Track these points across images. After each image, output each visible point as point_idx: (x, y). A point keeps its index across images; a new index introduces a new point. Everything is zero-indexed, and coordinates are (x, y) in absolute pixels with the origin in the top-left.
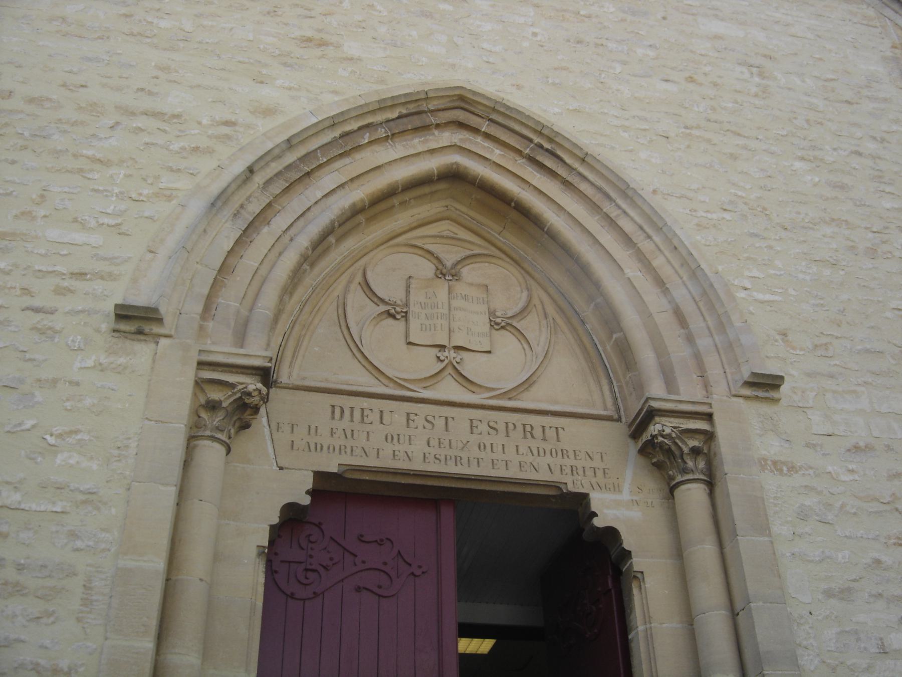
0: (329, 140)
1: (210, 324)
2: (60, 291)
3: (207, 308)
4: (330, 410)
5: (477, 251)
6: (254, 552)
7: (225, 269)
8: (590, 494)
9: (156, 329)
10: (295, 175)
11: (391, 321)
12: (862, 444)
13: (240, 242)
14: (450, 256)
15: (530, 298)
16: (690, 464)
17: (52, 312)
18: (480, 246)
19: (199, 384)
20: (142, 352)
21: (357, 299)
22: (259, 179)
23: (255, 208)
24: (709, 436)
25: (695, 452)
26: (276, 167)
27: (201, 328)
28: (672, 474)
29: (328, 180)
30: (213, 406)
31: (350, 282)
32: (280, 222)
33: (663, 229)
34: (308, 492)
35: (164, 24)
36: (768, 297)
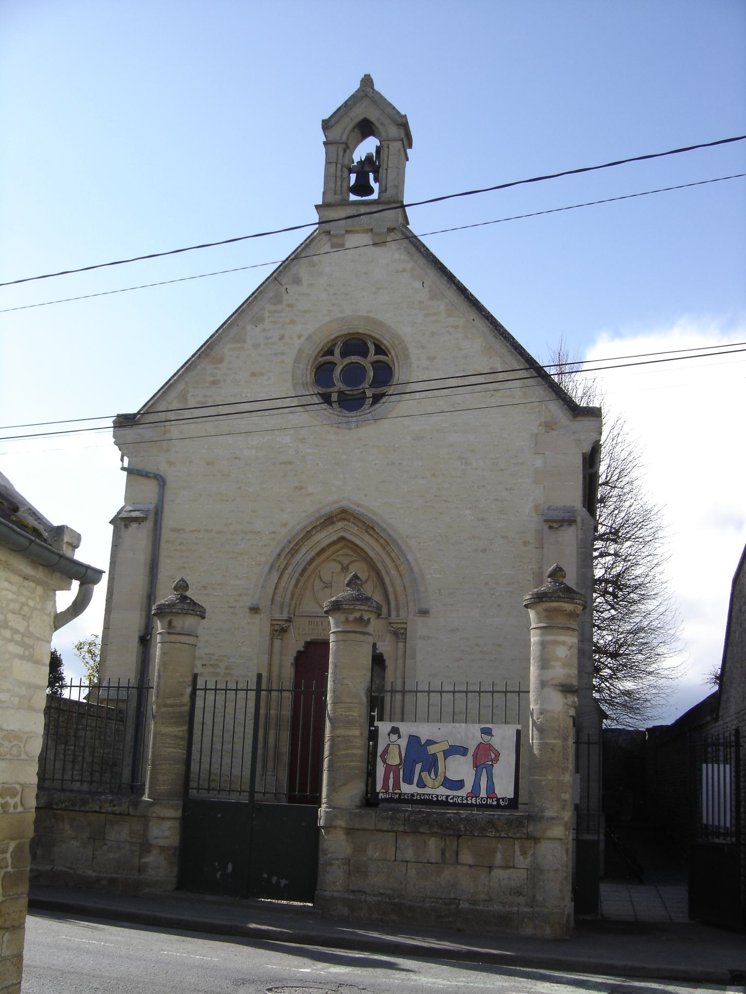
0: (302, 536)
1: (273, 606)
2: (236, 601)
3: (272, 602)
4: (308, 623)
5: (356, 559)
6: (290, 664)
7: (276, 588)
8: (377, 644)
9: (260, 612)
10: (293, 552)
11: (327, 589)
12: (454, 628)
13: (280, 578)
14: (346, 561)
15: (369, 575)
16: (401, 637)
17: (235, 607)
18: (355, 557)
19: (272, 625)
20: (258, 617)
21: (318, 582)
22: (283, 556)
23: (282, 566)
24: (406, 629)
25: (402, 634)
26: (287, 550)
27: (271, 608)
28: (130, 807)
29: (303, 550)
30: (276, 631)
31: (315, 577)
32: (290, 569)
33: (273, 693)
34: (303, 647)
35: (251, 490)
36: (438, 576)
